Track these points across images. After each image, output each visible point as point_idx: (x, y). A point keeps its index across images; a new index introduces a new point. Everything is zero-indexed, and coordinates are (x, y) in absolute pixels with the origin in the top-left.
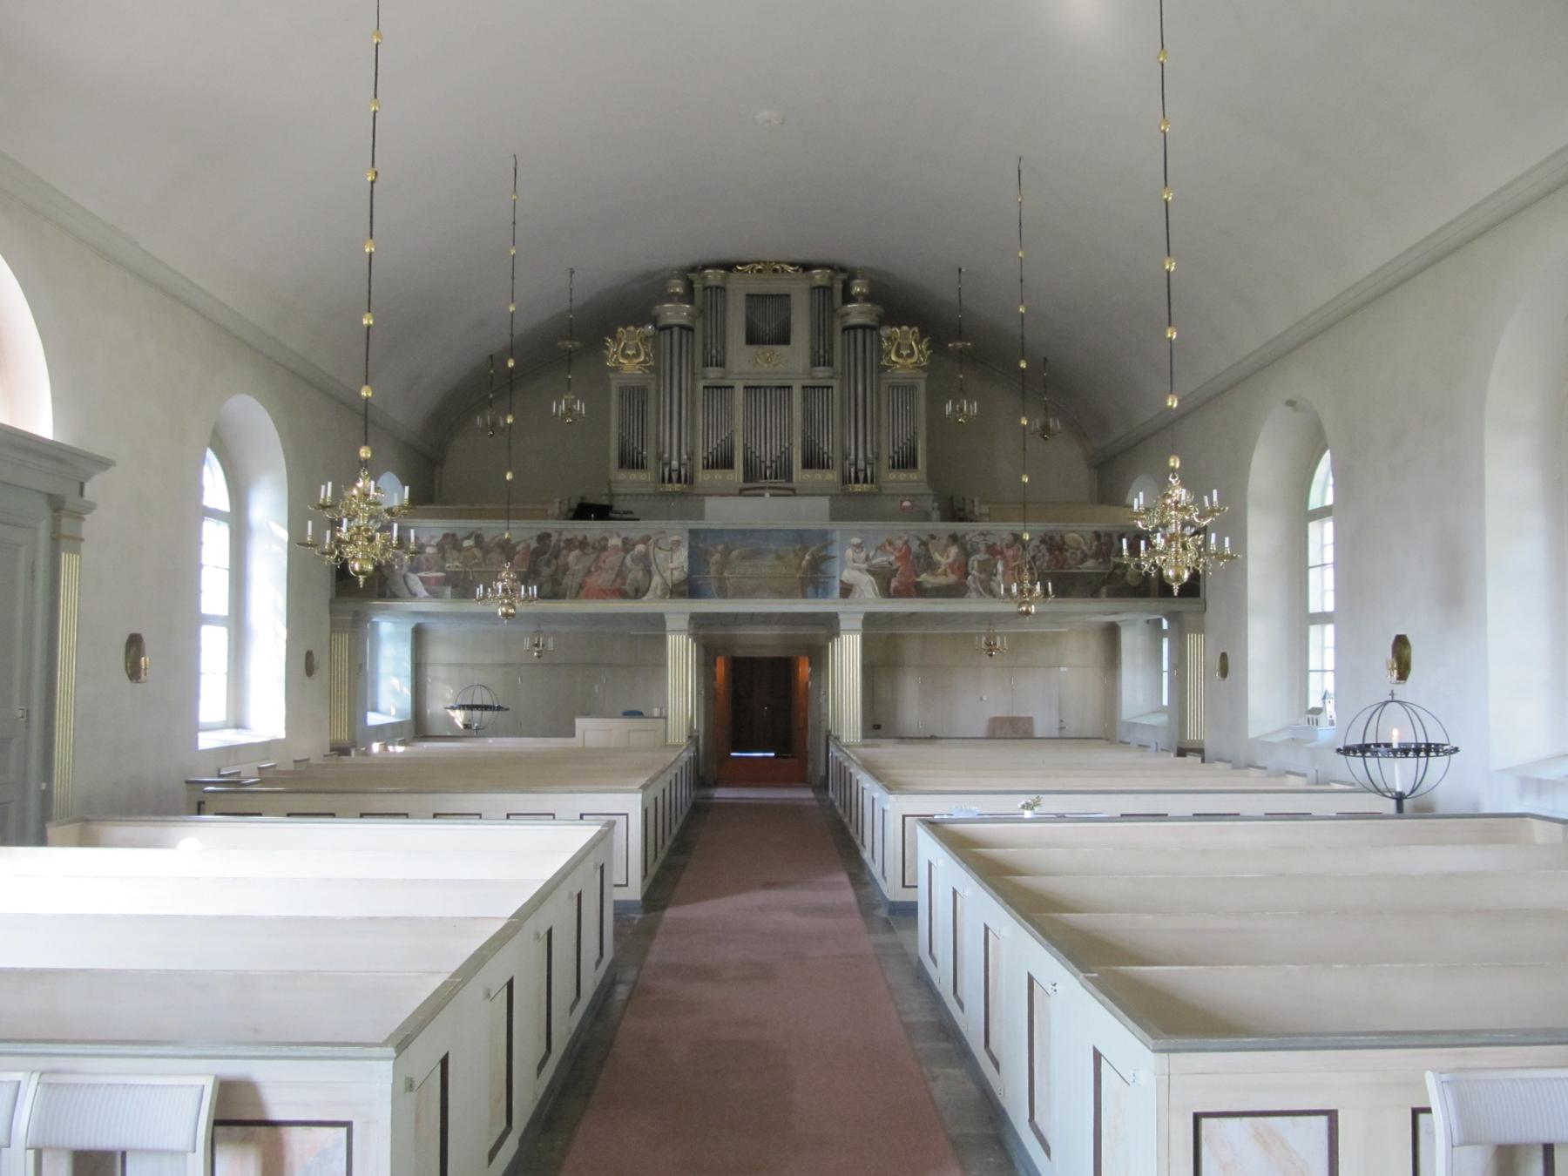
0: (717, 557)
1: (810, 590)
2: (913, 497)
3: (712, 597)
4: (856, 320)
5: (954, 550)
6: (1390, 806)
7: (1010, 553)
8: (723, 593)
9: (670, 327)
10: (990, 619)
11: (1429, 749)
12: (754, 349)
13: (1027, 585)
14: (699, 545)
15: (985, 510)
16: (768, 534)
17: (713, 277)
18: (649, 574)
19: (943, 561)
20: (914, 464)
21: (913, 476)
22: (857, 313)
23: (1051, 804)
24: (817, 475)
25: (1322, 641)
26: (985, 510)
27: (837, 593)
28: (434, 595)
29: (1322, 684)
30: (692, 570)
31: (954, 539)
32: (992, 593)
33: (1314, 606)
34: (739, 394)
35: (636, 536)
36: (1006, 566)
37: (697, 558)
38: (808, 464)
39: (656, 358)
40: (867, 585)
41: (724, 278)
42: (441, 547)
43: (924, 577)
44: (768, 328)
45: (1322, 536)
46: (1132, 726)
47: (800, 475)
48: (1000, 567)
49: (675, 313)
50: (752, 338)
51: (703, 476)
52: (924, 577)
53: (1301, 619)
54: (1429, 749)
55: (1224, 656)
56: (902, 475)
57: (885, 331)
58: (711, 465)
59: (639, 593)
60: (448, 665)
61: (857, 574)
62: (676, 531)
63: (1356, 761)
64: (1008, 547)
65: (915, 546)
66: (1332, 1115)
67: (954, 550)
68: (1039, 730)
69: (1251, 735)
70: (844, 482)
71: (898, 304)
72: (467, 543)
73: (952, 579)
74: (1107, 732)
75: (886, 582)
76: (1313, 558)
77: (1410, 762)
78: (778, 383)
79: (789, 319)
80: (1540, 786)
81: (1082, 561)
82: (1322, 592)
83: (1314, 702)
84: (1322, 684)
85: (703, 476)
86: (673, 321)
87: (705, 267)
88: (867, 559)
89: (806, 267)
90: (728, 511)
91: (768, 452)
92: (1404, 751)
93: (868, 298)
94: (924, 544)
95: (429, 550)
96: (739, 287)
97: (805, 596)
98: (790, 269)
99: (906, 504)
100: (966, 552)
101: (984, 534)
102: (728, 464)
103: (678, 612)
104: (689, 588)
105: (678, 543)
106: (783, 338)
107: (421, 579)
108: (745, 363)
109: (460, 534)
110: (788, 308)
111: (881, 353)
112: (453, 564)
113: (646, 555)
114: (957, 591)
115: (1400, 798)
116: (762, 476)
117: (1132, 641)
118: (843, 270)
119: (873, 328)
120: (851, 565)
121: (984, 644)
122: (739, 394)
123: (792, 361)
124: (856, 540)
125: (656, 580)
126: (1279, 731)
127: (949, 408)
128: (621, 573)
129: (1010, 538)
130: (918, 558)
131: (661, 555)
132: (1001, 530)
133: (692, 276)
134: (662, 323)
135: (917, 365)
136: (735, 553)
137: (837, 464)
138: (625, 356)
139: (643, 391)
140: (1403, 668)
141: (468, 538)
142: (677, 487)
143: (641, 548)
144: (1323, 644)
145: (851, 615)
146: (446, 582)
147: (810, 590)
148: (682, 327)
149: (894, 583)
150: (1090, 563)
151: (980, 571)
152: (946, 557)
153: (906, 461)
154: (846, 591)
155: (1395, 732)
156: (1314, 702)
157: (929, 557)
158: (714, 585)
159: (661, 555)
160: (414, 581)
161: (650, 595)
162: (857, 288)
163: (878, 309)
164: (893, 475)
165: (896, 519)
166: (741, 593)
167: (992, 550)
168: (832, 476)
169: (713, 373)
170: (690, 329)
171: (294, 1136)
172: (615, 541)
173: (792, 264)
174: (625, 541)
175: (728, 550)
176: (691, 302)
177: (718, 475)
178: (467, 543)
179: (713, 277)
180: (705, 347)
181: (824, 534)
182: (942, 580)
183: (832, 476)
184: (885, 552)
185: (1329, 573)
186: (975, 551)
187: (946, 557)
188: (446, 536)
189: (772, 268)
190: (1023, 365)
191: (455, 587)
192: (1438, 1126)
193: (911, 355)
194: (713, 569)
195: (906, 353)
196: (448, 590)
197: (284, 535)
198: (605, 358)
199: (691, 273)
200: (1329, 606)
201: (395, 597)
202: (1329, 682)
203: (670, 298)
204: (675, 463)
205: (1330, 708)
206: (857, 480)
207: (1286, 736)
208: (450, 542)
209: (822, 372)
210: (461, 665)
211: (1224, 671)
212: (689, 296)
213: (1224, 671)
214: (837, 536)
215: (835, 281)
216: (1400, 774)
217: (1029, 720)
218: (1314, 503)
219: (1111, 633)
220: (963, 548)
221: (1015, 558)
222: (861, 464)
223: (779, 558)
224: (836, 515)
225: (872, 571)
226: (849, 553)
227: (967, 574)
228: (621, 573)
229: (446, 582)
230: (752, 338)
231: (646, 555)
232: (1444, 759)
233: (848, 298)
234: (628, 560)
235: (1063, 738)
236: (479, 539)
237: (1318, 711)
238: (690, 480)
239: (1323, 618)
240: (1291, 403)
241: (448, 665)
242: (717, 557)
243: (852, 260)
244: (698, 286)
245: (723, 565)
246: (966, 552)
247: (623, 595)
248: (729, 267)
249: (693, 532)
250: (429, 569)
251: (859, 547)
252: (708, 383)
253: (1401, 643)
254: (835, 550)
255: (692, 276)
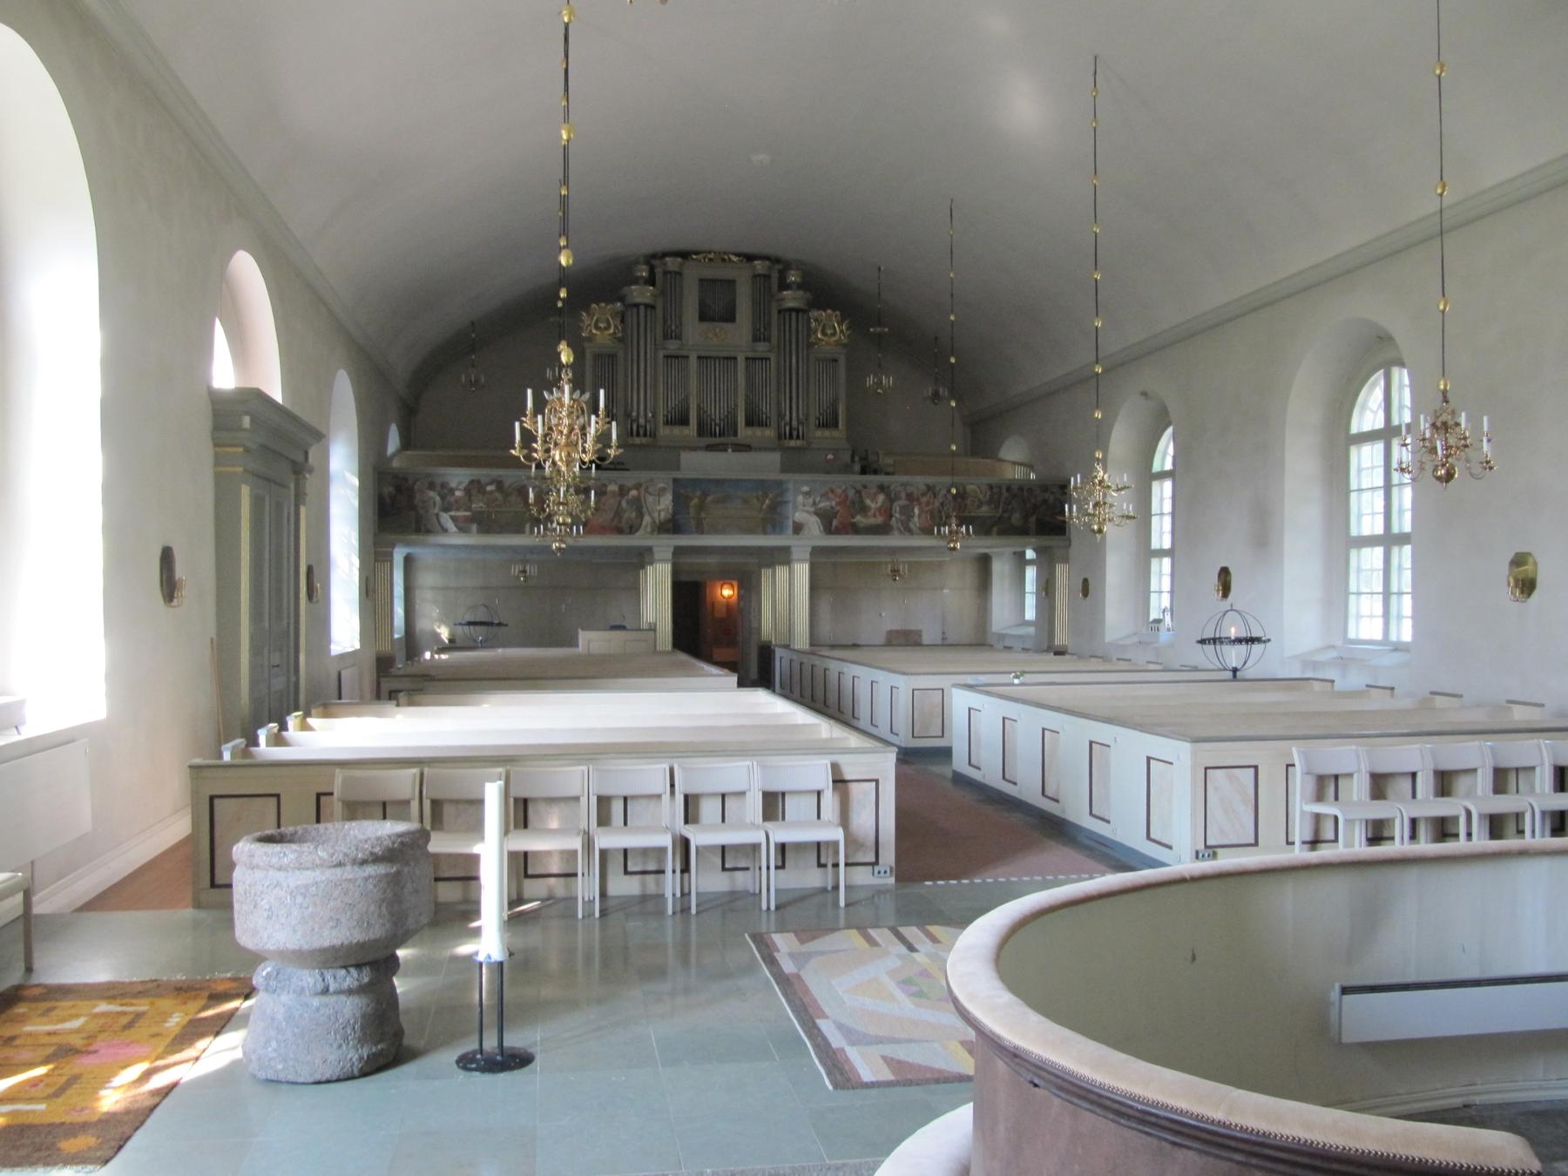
0: (695, 501)
1: (769, 528)
2: (835, 451)
3: (690, 533)
4: (791, 304)
5: (881, 497)
6: (1229, 675)
7: (924, 499)
8: (700, 530)
9: (637, 305)
10: (893, 551)
11: (1252, 640)
12: (706, 325)
13: (954, 527)
14: (682, 491)
15: (889, 461)
16: (737, 483)
17: (672, 263)
18: (641, 515)
19: (873, 505)
20: (836, 425)
21: (835, 433)
22: (792, 299)
23: (1028, 678)
24: (758, 431)
25: (1162, 570)
26: (889, 461)
27: (790, 530)
28: (463, 530)
29: (1160, 602)
30: (675, 513)
31: (882, 488)
32: (910, 531)
33: (1155, 545)
34: (693, 361)
35: (630, 483)
36: (921, 510)
37: (680, 501)
38: (750, 423)
39: (624, 330)
40: (813, 524)
41: (681, 265)
42: (468, 491)
43: (858, 518)
44: (717, 310)
45: (1163, 493)
46: (1002, 637)
47: (744, 433)
48: (916, 511)
49: (640, 294)
50: (703, 317)
51: (664, 432)
52: (858, 518)
53: (1146, 554)
54: (1252, 640)
55: (1085, 581)
56: (827, 433)
57: (814, 314)
58: (669, 422)
59: (632, 529)
60: (433, 588)
61: (805, 515)
62: (662, 479)
63: (1209, 648)
64: (924, 494)
65: (851, 493)
66: (1256, 767)
67: (881, 497)
68: (926, 640)
69: (1108, 639)
70: (779, 437)
71: (825, 291)
72: (489, 488)
73: (879, 520)
74: (980, 640)
75: (830, 523)
76: (1155, 508)
77: (1243, 648)
78: (725, 354)
79: (734, 300)
80: (1315, 665)
81: (979, 506)
82: (1162, 534)
83: (1154, 615)
84: (1160, 602)
85: (664, 432)
86: (638, 300)
87: (665, 254)
88: (814, 504)
89: (750, 258)
90: (700, 464)
91: (716, 413)
92: (1239, 641)
93: (800, 286)
94: (858, 492)
95: (458, 493)
96: (693, 273)
97: (765, 532)
98: (734, 259)
99: (830, 456)
100: (891, 499)
101: (904, 485)
102: (683, 421)
103: (664, 545)
104: (672, 526)
105: (663, 490)
106: (730, 317)
107: (453, 518)
108: (695, 334)
109: (483, 480)
110: (734, 293)
111: (810, 332)
112: (478, 505)
113: (637, 500)
114: (882, 529)
115: (1235, 670)
116: (717, 435)
117: (1001, 569)
118: (777, 261)
119: (804, 311)
120: (802, 510)
121: (900, 572)
122: (693, 361)
123: (737, 335)
124: (806, 489)
125: (647, 519)
126: (1128, 637)
127: (870, 381)
128: (618, 513)
129: (924, 488)
130: (853, 503)
131: (650, 499)
132: (920, 481)
133: (654, 262)
134: (629, 300)
135: (838, 343)
136: (710, 498)
137: (774, 424)
138: (597, 328)
139: (612, 357)
140: (1226, 589)
141: (491, 483)
142: (644, 440)
143: (634, 493)
144: (1162, 573)
145: (801, 547)
146: (471, 520)
147: (769, 528)
148: (646, 306)
149: (835, 523)
150: (985, 508)
151: (901, 513)
152: (876, 502)
153: (830, 422)
154: (798, 528)
155: (1233, 630)
156: (1154, 615)
157: (862, 502)
158: (693, 523)
159: (650, 499)
160: (446, 518)
161: (641, 531)
162: (793, 278)
163: (808, 295)
164: (819, 433)
165: (817, 471)
166: (715, 530)
167: (910, 497)
168: (770, 433)
169: (672, 346)
170: (653, 307)
171: (854, 787)
172: (613, 488)
173: (737, 255)
174: (621, 488)
175: (705, 495)
176: (653, 284)
177: (677, 431)
178: (489, 488)
179: (672, 263)
180: (665, 322)
181: (780, 483)
182: (872, 521)
183: (770, 433)
184: (829, 499)
185: (1167, 521)
186: (898, 498)
187: (876, 502)
188: (472, 482)
189: (722, 258)
190: (953, 360)
191: (480, 523)
192: (1298, 771)
193: (834, 334)
194: (692, 511)
195: (830, 330)
196: (474, 527)
197: (356, 482)
198: (581, 328)
199: (652, 259)
200: (1167, 545)
201: (428, 532)
202: (1166, 601)
203: (636, 281)
204: (642, 421)
205: (1168, 618)
206: (791, 437)
207: (1136, 639)
208: (475, 487)
209: (762, 347)
210: (447, 588)
211: (1086, 592)
212: (651, 281)
213: (1086, 592)
214: (791, 486)
215: (773, 270)
216: (1234, 655)
217: (919, 633)
218: (1156, 467)
219: (984, 562)
220: (888, 495)
221: (928, 503)
222: (794, 423)
223: (745, 501)
224: (785, 469)
225: (816, 513)
226: (800, 498)
227: (891, 516)
228: (618, 513)
229: (471, 520)
230: (703, 317)
231: (637, 500)
232: (1262, 646)
233: (783, 285)
234: (624, 504)
235: (946, 645)
236: (499, 484)
237: (1158, 621)
238: (653, 435)
239: (1161, 553)
240: (1144, 394)
241: (433, 588)
242: (695, 501)
243: (790, 255)
244: (659, 271)
245: (701, 507)
246: (891, 499)
247: (620, 531)
248: (684, 255)
249: (675, 480)
250: (458, 509)
251: (808, 494)
252: (667, 352)
253: (1224, 573)
254: (789, 496)
255: (654, 262)
